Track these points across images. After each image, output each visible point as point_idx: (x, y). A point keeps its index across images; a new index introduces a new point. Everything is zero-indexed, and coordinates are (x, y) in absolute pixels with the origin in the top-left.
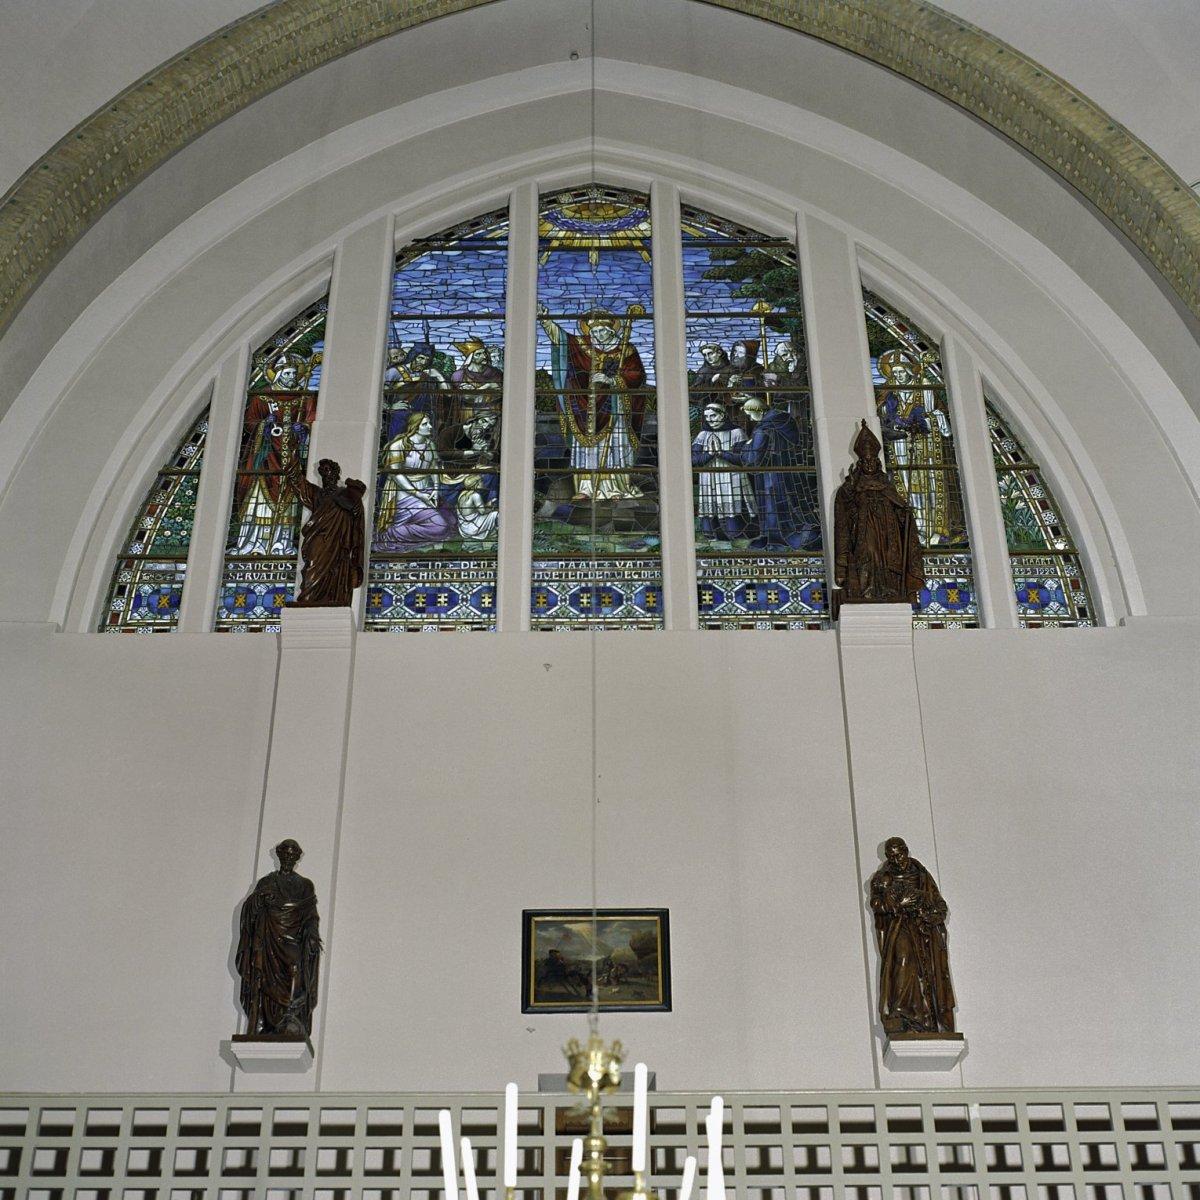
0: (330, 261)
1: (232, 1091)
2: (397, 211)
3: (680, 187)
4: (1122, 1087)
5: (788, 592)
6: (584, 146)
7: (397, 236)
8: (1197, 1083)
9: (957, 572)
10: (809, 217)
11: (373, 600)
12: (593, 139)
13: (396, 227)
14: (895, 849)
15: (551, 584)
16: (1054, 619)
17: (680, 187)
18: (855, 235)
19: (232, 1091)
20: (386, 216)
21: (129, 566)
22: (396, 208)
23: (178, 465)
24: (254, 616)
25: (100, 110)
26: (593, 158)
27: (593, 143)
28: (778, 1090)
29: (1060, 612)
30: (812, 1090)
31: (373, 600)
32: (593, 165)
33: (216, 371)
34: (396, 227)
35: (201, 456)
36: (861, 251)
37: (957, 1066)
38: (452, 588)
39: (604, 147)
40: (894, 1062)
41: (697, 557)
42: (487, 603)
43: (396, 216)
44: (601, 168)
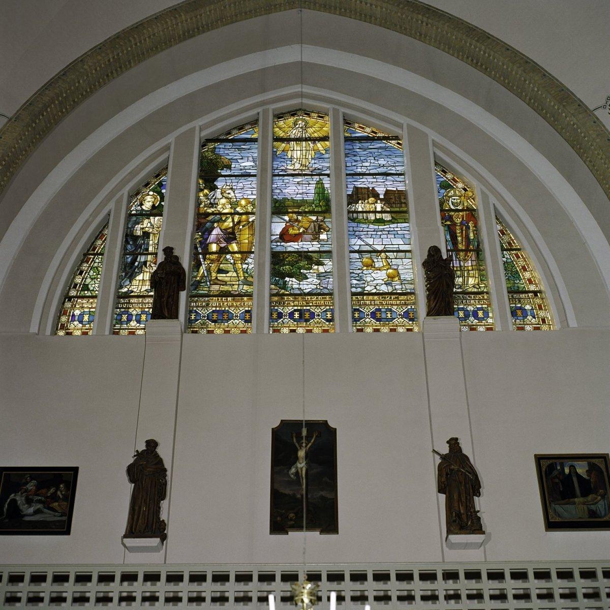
0: (167, 148)
1: (165, 563)
2: (201, 124)
3: (343, 110)
4: (555, 561)
5: (233, 314)
6: (297, 89)
7: (201, 135)
8: (609, 559)
9: (484, 302)
10: (408, 125)
11: (331, 315)
12: (302, 86)
13: (201, 130)
14: (152, 445)
15: (312, 307)
16: (126, 329)
17: (343, 110)
18: (433, 135)
19: (165, 563)
20: (195, 127)
21: (70, 300)
22: (198, 123)
23: (92, 250)
24: (470, 322)
25: (543, 69)
26: (302, 95)
27: (302, 88)
28: (312, 563)
29: (532, 321)
30: (331, 563)
31: (331, 315)
32: (302, 100)
33: (111, 205)
34: (201, 130)
35: (104, 247)
36: (435, 144)
37: (482, 548)
38: (197, 310)
39: (307, 89)
40: (452, 546)
41: (352, 295)
42: (275, 317)
43: (200, 126)
44: (305, 101)
